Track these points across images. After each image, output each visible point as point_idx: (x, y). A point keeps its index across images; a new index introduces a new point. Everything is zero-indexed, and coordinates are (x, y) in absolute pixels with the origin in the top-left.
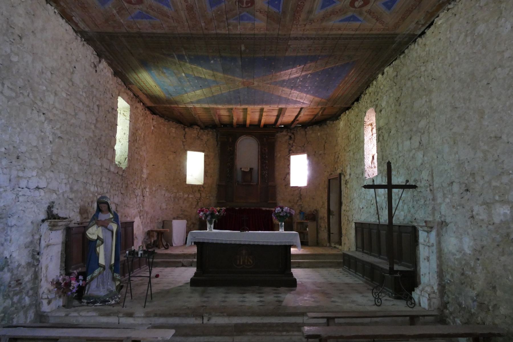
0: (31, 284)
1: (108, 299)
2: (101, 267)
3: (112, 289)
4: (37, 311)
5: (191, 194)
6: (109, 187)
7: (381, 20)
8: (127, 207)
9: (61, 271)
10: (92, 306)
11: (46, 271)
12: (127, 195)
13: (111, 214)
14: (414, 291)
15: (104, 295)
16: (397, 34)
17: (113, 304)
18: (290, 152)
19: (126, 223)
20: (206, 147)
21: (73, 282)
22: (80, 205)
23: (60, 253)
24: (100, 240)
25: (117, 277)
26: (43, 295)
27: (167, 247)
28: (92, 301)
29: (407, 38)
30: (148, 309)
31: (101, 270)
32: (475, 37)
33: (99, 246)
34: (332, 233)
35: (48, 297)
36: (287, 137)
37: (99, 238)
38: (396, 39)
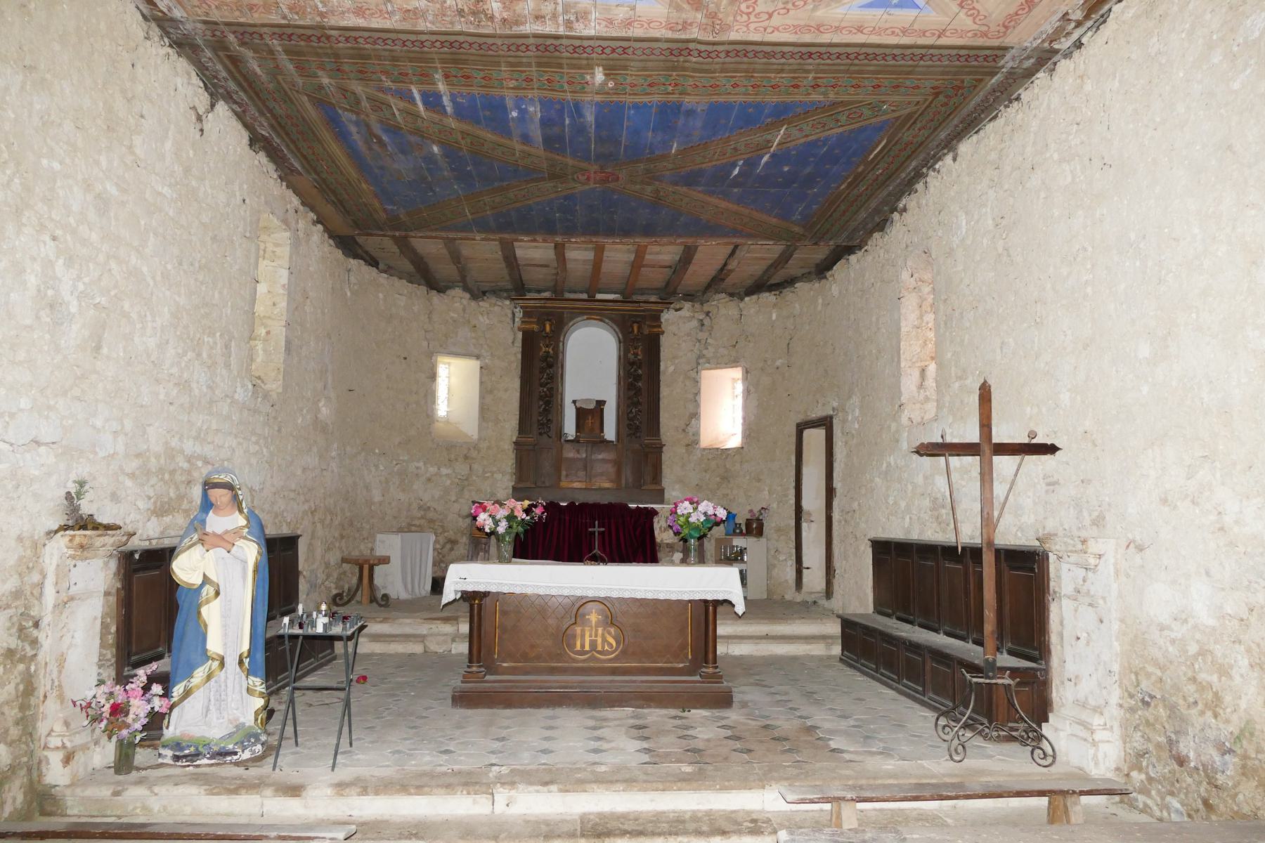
0: (16, 710)
2: (213, 659)
3: (242, 720)
4: (31, 782)
5: (445, 465)
7: (971, 7)
9: (101, 671)
10: (189, 766)
11: (60, 672)
14: (1047, 720)
16: (1006, 49)
18: (701, 361)
20: (486, 346)
21: (134, 702)
23: (99, 622)
26: (49, 738)
27: (383, 603)
29: (1032, 61)
30: (344, 773)
31: (213, 668)
32: (1235, 49)
33: (208, 602)
34: (808, 568)
35: (63, 744)
36: (695, 323)
37: (206, 581)
38: (1002, 62)
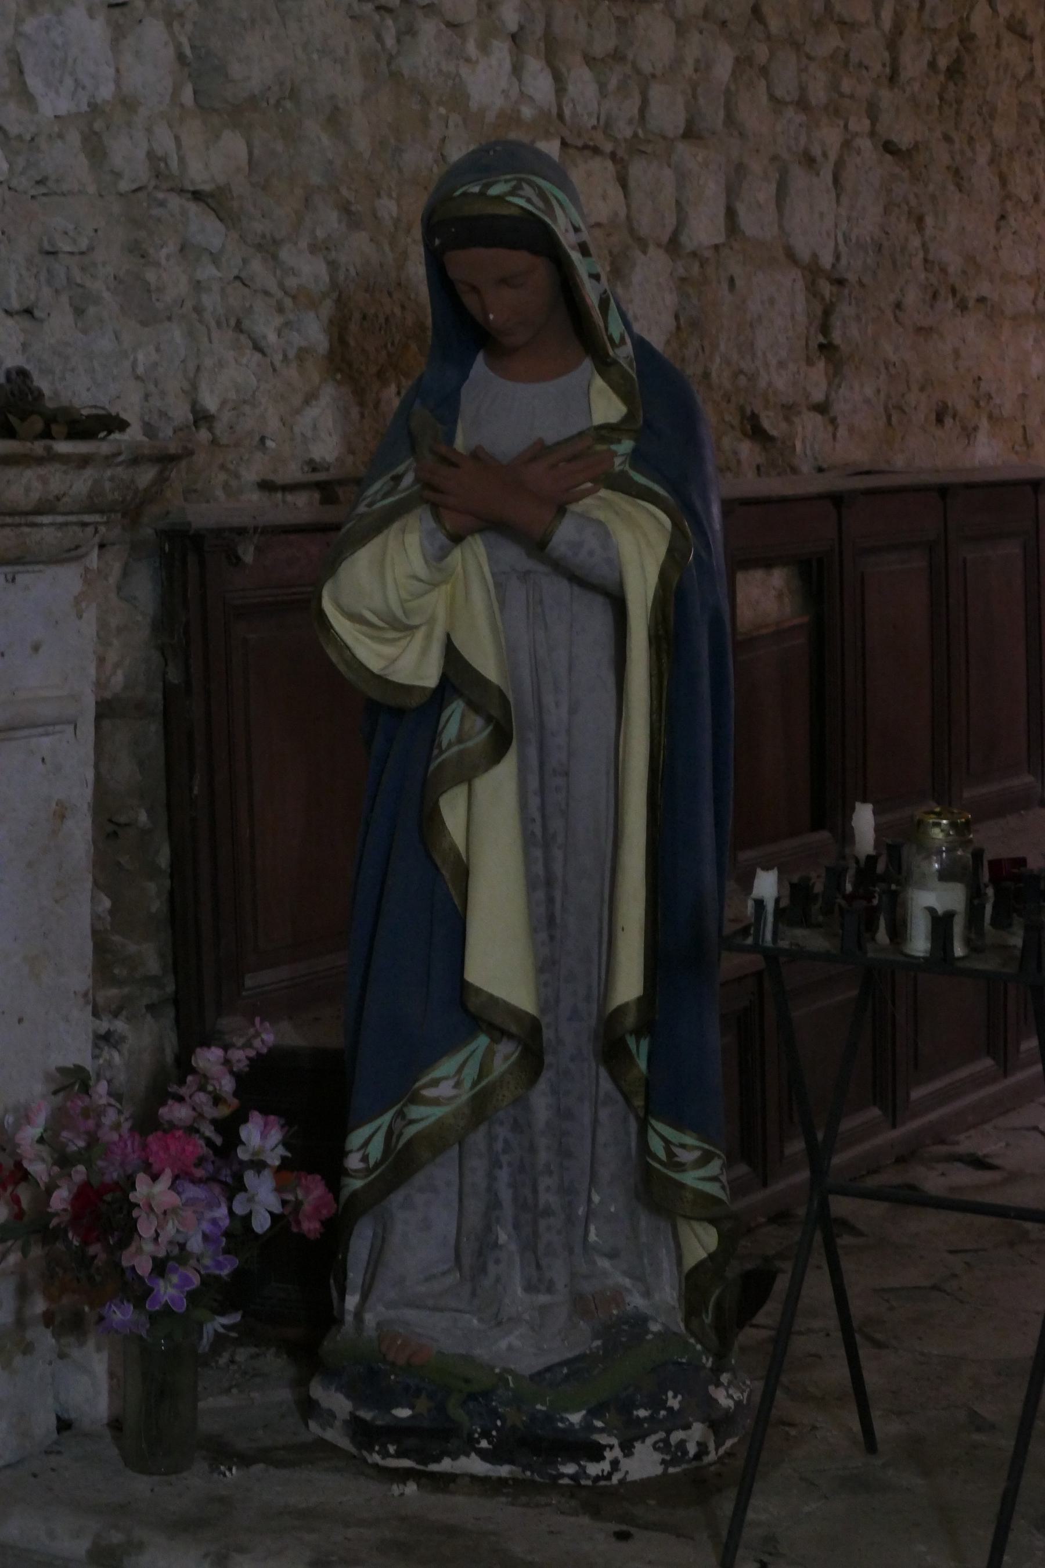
1: (576, 1418)
2: (498, 1033)
3: (636, 1301)
6: (723, 70)
8: (963, 306)
12: (957, 173)
13: (599, 383)
15: (538, 1364)
17: (646, 1486)
19: (944, 491)
22: (333, 266)
24: (474, 706)
25: (680, 1167)
28: (404, 1413)
